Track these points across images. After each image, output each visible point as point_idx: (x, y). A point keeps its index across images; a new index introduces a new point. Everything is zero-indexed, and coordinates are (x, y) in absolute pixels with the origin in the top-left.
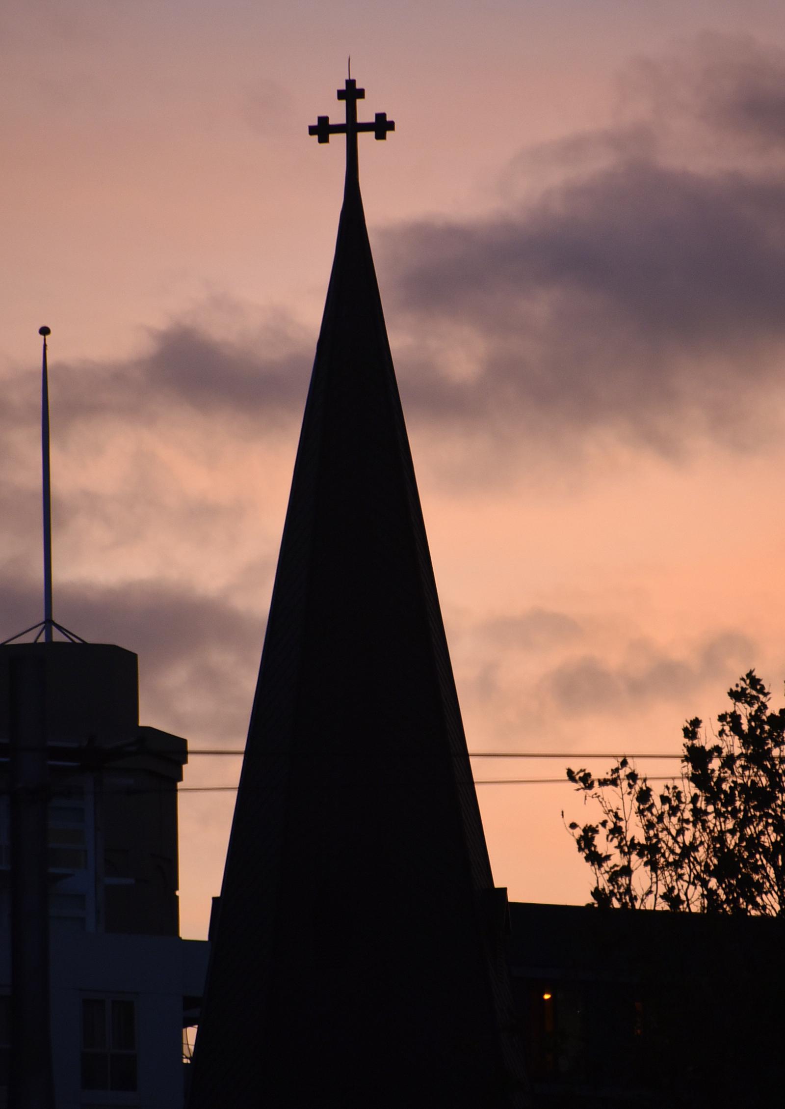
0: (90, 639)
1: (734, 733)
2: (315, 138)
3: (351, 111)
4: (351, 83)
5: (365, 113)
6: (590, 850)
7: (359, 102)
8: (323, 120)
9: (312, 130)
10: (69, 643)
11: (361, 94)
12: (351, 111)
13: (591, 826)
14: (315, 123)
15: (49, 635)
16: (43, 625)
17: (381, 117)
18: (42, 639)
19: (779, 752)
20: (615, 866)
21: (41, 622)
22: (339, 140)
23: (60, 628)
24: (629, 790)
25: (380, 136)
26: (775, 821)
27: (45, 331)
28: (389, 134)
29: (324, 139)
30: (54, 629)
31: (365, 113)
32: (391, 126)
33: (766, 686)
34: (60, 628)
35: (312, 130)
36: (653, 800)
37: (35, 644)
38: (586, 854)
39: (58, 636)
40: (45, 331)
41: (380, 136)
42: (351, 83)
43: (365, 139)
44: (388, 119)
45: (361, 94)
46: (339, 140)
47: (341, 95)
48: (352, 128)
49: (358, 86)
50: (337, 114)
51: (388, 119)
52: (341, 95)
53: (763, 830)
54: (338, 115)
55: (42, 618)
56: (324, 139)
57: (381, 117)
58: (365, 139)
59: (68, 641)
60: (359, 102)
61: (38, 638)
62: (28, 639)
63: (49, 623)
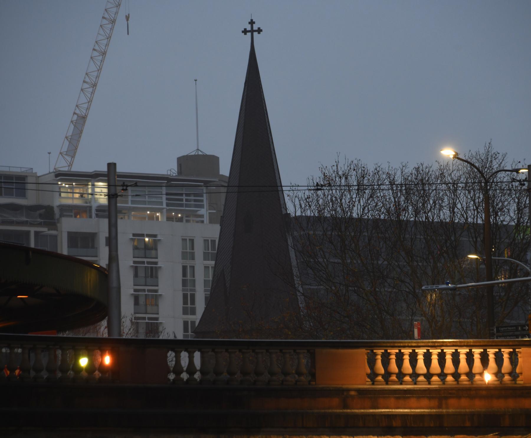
0: (208, 154)
1: (198, 155)
2: (243, 34)
4: (252, 20)
5: (255, 27)
6: (336, 212)
7: (254, 25)
8: (245, 29)
9: (243, 32)
10: (202, 155)
11: (254, 23)
13: (36, 173)
14: (243, 30)
16: (456, 204)
17: (259, 28)
18: (196, 154)
19: (458, 207)
20: (366, 350)
21: (195, 150)
22: (249, 34)
25: (259, 33)
26: (116, 177)
27: (196, 80)
28: (261, 32)
29: (245, 34)
30: (199, 151)
31: (255, 27)
32: (261, 31)
34: (201, 151)
35: (243, 32)
38: (438, 221)
39: (200, 153)
40: (196, 80)
41: (259, 33)
42: (252, 20)
43: (255, 34)
44: (261, 29)
45: (254, 23)
46: (249, 34)
47: (249, 23)
48: (252, 31)
49: (254, 21)
50: (249, 28)
52: (249, 23)
56: (245, 34)
57: (259, 28)
58: (255, 34)
59: (202, 154)
60: (254, 25)
61: (195, 153)
62: (193, 154)
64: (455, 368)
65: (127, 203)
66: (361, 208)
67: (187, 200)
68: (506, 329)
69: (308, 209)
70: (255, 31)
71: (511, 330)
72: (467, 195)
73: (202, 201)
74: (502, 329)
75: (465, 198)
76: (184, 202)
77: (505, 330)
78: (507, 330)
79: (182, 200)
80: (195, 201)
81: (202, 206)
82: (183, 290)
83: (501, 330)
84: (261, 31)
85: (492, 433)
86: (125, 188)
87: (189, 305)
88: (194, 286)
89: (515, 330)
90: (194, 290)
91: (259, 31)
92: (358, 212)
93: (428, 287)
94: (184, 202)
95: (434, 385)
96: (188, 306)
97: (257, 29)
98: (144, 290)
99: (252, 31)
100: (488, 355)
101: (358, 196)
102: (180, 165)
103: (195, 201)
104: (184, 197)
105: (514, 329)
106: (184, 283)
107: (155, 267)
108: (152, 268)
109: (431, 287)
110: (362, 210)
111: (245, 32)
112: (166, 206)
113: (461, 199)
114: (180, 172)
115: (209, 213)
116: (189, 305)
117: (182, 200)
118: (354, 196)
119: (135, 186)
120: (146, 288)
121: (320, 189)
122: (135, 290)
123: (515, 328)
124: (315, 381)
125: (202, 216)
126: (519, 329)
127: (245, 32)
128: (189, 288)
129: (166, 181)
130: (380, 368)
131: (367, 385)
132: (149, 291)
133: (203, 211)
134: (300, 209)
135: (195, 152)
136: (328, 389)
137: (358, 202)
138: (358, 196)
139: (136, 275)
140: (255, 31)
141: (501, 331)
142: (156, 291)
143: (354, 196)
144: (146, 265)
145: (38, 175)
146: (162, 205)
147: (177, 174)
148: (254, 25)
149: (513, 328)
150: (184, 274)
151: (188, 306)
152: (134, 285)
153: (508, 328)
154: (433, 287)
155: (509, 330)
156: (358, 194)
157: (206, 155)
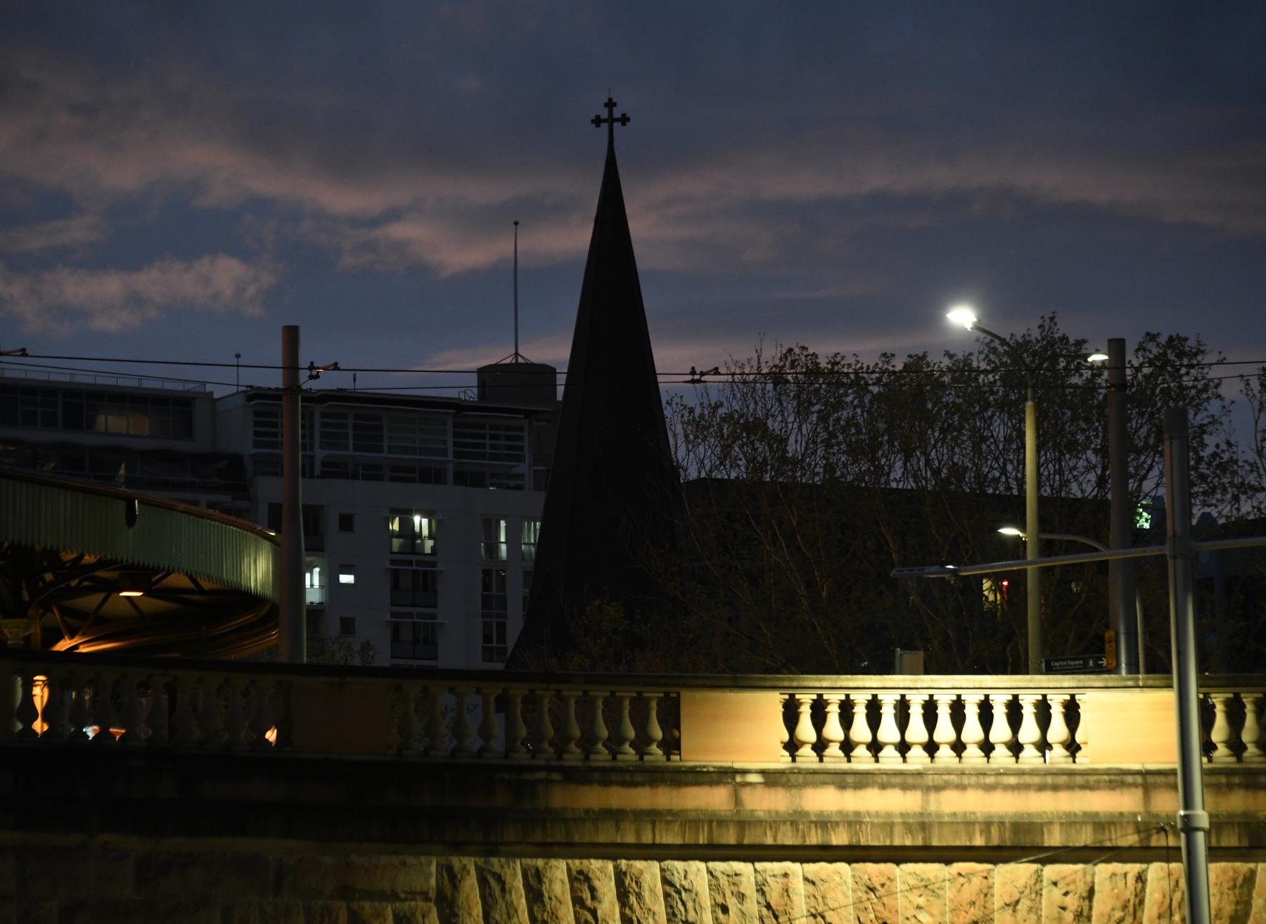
3: (611, 113)
4: (610, 100)
5: (617, 113)
8: (598, 117)
9: (593, 121)
11: (615, 105)
12: (611, 113)
15: (517, 360)
17: (624, 115)
20: (781, 694)
22: (605, 126)
23: (521, 356)
24: (800, 345)
27: (516, 223)
31: (617, 113)
32: (628, 119)
33: (917, 353)
34: (521, 356)
35: (593, 121)
36: (761, 810)
37: (511, 364)
39: (520, 360)
40: (516, 223)
41: (624, 124)
42: (610, 100)
43: (617, 125)
44: (627, 123)
45: (615, 105)
46: (605, 126)
47: (606, 105)
48: (611, 120)
50: (604, 114)
51: (627, 123)
52: (606, 105)
53: (675, 758)
54: (604, 115)
55: (514, 352)
57: (624, 115)
58: (617, 125)
62: (508, 361)
63: (517, 354)
64: (957, 734)
65: (382, 452)
66: (803, 439)
67: (493, 447)
68: (1065, 663)
69: (700, 444)
70: (617, 120)
71: (1075, 665)
72: (1006, 421)
73: (521, 448)
74: (1057, 664)
75: (1002, 426)
76: (488, 450)
77: (1063, 666)
78: (1067, 665)
79: (483, 446)
80: (508, 448)
81: (520, 459)
82: (484, 616)
83: (1056, 666)
84: (628, 119)
85: (1025, 857)
86: (314, 373)
87: (495, 644)
88: (505, 609)
89: (1081, 667)
90: (505, 616)
91: (624, 120)
92: (796, 449)
93: (902, 571)
94: (488, 450)
95: (913, 763)
96: (491, 645)
97: (620, 116)
98: (410, 615)
99: (611, 120)
100: (1021, 707)
101: (798, 420)
102: (482, 385)
103: (508, 448)
104: (488, 442)
105: (1080, 664)
106: (486, 602)
107: (433, 572)
108: (425, 572)
109: (909, 570)
110: (804, 444)
111: (597, 121)
112: (454, 457)
113: (995, 429)
114: (482, 396)
115: (535, 471)
116: (495, 644)
117: (483, 446)
118: (791, 419)
119: (334, 369)
120: (414, 610)
121: (699, 381)
122: (393, 615)
123: (1081, 662)
124: (680, 755)
125: (521, 476)
126: (1089, 663)
127: (597, 121)
128: (495, 611)
129: (454, 411)
130: (806, 730)
131: (782, 761)
132: (419, 615)
133: (523, 468)
134: (684, 443)
135: (512, 358)
136: (705, 770)
137: (797, 430)
138: (798, 420)
139: (395, 586)
140: (617, 120)
141: (1054, 668)
142: (433, 617)
143: (791, 419)
144: (415, 567)
145: (216, 396)
146: (446, 455)
147: (476, 400)
148: (614, 109)
149: (1077, 662)
150: (486, 586)
151: (491, 645)
152: (393, 605)
153: (1069, 663)
154: (913, 570)
155: (1071, 665)
156: (798, 413)
157: (532, 364)
